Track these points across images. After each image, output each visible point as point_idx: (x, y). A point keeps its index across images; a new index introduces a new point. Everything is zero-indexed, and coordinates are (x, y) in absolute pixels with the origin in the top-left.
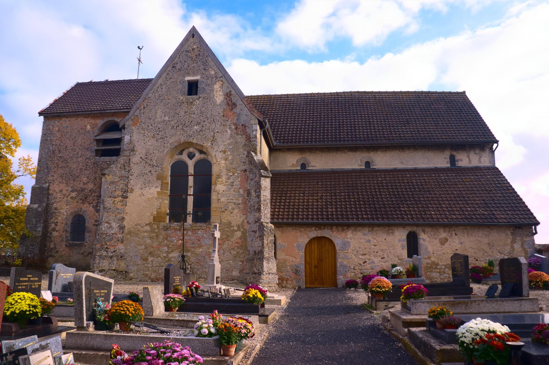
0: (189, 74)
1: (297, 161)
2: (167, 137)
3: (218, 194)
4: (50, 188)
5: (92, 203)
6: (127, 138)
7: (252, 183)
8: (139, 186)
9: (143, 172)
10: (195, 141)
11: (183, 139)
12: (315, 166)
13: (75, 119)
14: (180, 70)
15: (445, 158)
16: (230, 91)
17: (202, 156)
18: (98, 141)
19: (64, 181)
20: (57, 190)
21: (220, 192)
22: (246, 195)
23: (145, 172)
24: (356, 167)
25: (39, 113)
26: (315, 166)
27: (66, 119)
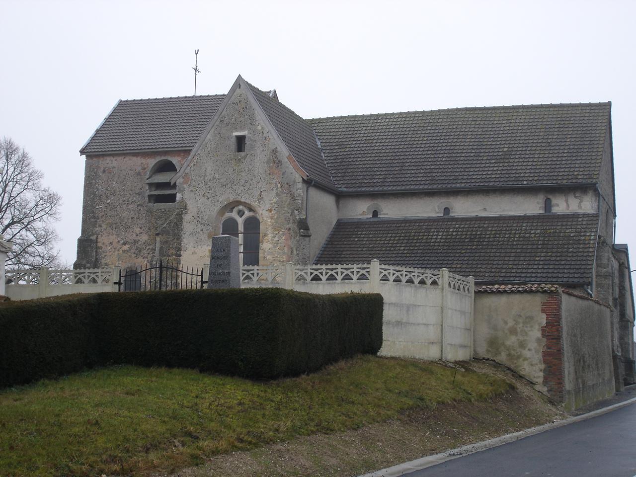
0: (236, 129)
1: (368, 209)
2: (217, 196)
3: (265, 251)
4: (99, 240)
5: (147, 257)
6: (179, 196)
7: (294, 242)
8: (192, 244)
9: (195, 230)
10: (243, 200)
11: (232, 198)
12: (387, 214)
13: (122, 158)
14: (227, 124)
15: (538, 203)
16: (276, 148)
17: (251, 214)
18: (151, 185)
19: (114, 232)
20: (107, 243)
21: (266, 250)
22: (289, 254)
23: (198, 230)
24: (433, 215)
25: (80, 152)
26: (387, 214)
27: (112, 158)
